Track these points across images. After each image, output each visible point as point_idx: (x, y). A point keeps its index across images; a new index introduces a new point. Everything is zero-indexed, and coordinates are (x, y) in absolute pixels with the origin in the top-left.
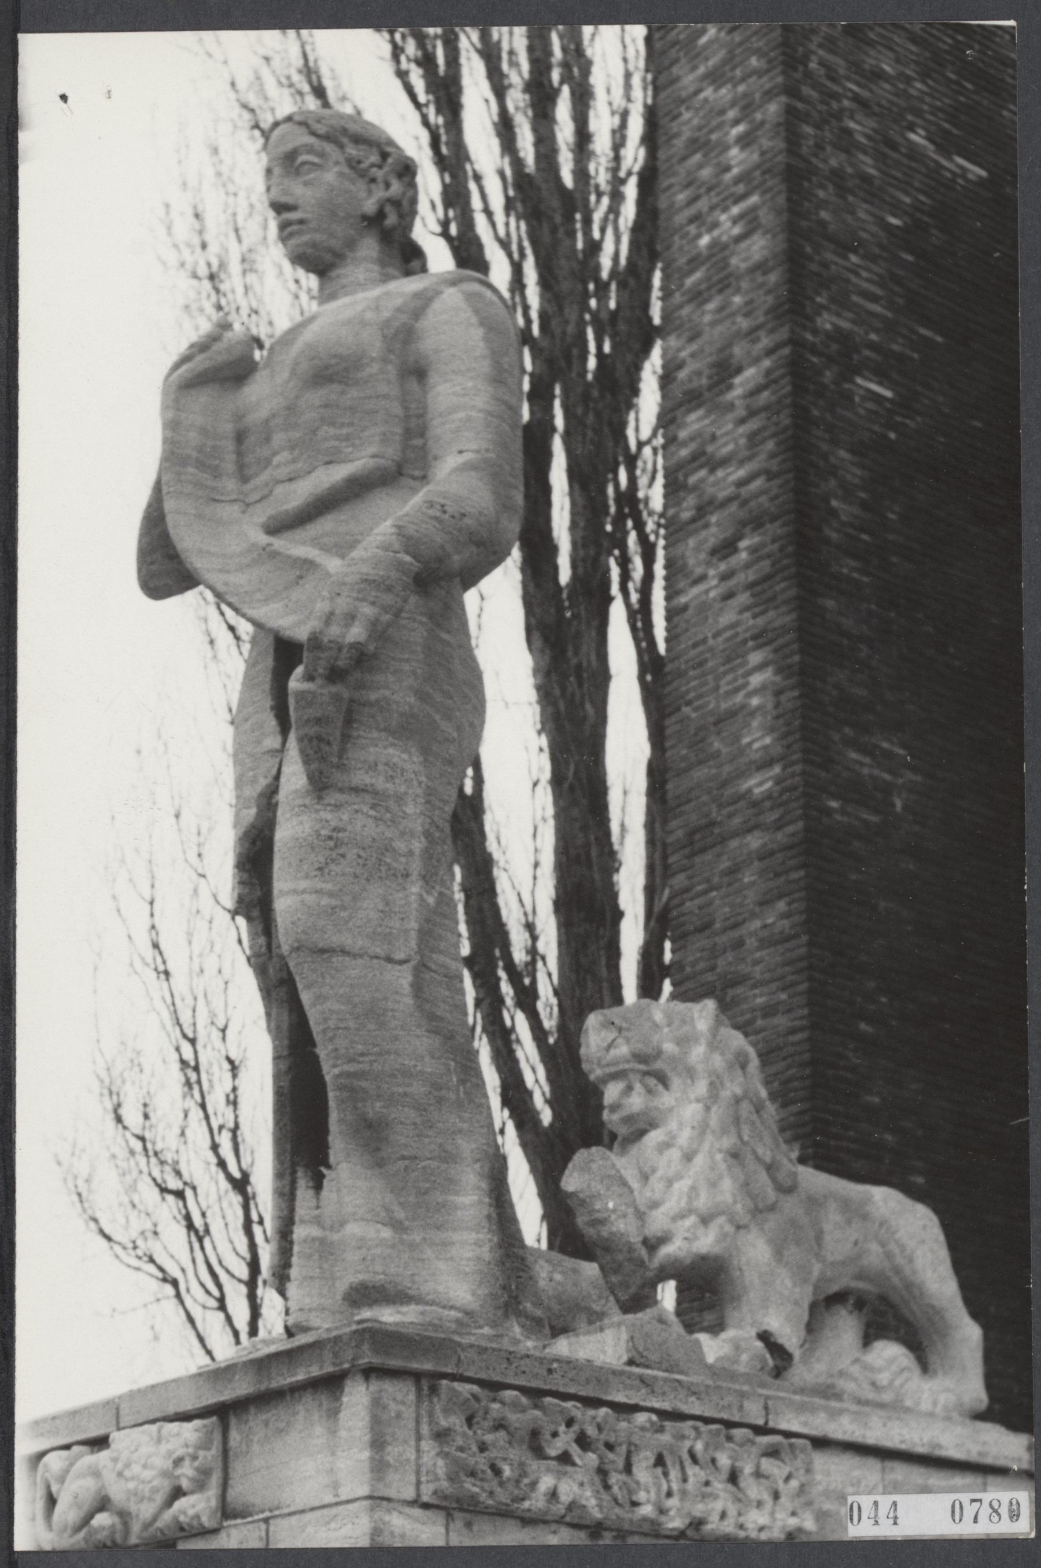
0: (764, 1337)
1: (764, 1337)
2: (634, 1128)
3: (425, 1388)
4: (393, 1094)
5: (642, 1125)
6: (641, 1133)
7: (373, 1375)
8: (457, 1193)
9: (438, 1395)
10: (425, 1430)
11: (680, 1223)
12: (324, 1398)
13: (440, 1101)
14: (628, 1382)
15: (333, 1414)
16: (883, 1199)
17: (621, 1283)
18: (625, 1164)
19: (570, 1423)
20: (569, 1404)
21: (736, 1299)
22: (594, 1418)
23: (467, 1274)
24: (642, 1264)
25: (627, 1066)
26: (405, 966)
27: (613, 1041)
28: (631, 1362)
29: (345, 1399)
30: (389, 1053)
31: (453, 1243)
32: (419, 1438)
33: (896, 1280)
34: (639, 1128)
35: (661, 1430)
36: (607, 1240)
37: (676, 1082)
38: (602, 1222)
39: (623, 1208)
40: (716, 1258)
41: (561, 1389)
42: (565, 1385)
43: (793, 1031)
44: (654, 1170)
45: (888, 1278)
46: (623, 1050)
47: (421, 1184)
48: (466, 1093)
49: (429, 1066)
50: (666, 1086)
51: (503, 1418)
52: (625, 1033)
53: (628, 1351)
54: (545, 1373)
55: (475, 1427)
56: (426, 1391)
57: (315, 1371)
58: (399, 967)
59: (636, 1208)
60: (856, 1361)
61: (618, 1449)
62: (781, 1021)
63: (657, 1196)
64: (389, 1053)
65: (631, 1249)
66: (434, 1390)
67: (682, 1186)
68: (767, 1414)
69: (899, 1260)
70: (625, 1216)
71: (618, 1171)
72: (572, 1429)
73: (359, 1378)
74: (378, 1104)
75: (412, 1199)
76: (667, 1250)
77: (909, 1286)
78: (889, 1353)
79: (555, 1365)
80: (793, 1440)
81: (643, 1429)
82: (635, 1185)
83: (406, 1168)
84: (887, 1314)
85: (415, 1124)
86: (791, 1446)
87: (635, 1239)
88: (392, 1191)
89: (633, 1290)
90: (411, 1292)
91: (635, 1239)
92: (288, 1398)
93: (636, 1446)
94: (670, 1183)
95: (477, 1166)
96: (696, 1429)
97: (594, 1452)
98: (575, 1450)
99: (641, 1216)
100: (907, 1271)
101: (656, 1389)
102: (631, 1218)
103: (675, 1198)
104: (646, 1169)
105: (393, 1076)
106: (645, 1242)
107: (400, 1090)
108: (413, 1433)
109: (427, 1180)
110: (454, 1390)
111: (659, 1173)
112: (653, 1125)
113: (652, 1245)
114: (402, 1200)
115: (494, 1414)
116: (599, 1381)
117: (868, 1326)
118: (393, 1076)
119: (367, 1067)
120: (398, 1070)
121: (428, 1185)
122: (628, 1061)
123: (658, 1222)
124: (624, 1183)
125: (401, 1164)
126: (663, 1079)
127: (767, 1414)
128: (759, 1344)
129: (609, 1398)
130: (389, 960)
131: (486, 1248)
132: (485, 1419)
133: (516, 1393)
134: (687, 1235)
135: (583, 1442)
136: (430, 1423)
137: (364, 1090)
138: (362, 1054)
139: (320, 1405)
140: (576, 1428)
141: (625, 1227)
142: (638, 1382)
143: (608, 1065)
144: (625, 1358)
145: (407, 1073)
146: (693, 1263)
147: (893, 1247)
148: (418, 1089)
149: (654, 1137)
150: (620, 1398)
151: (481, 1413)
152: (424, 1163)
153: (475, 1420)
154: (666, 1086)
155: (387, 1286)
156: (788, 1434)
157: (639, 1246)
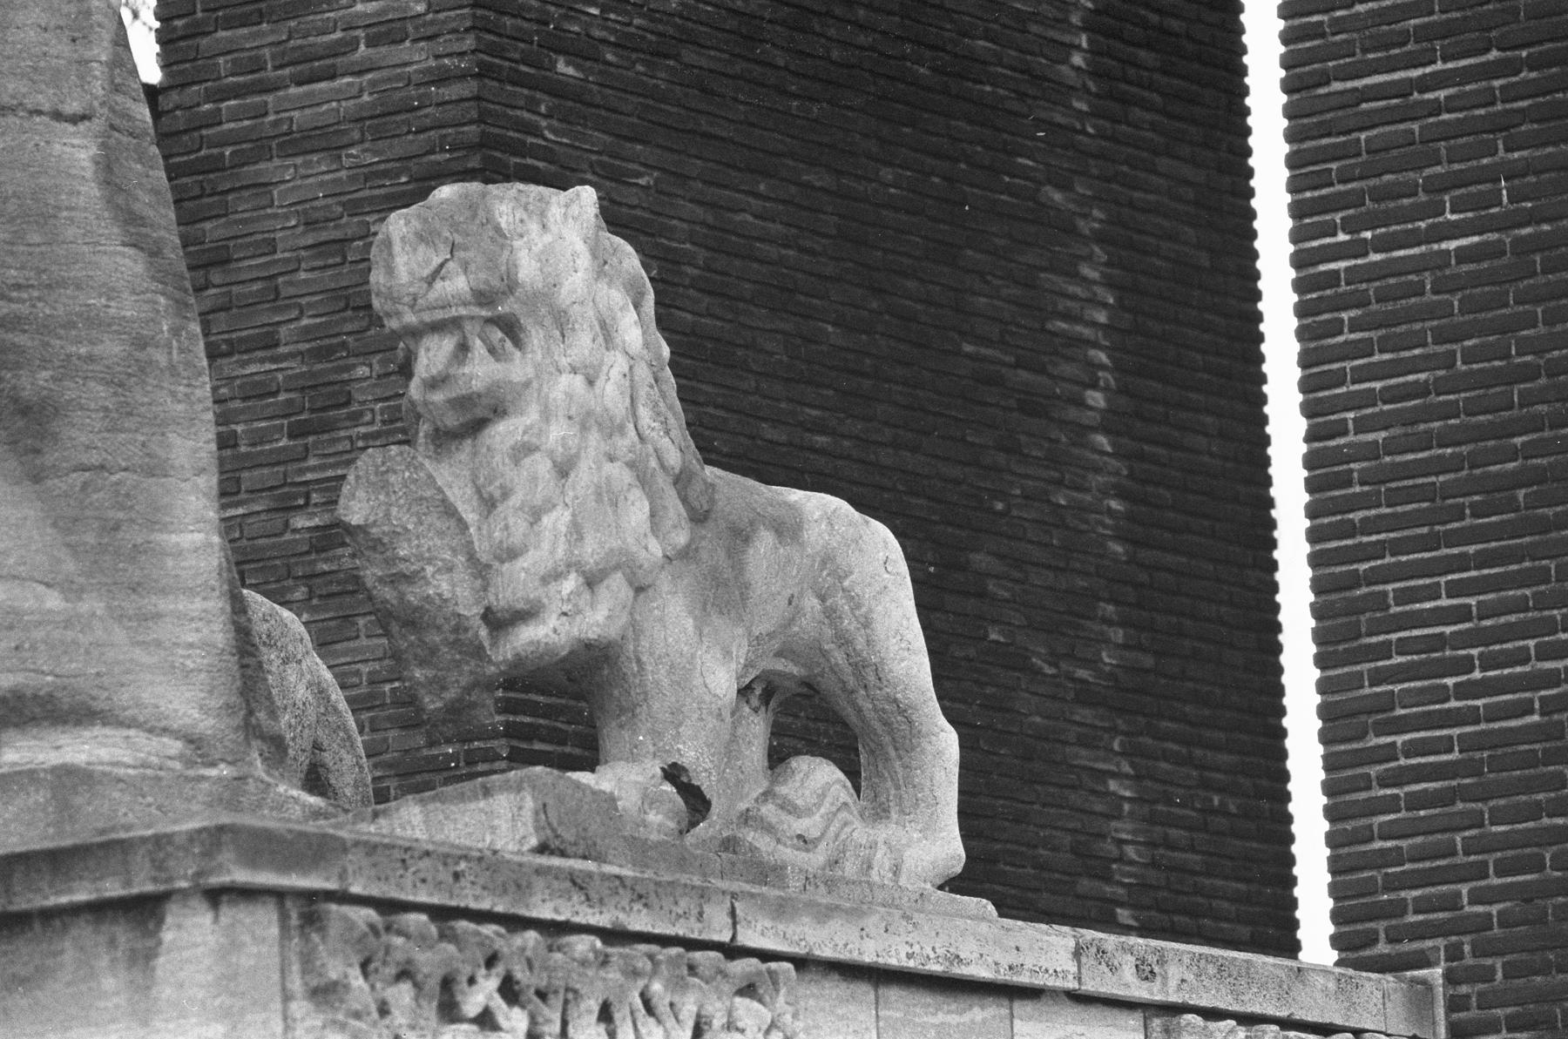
0: (673, 774)
1: (673, 774)
2: (469, 416)
3: (294, 915)
4: (69, 356)
5: (480, 413)
6: (477, 426)
7: (225, 898)
8: (165, 528)
9: (322, 929)
10: (296, 984)
11: (553, 587)
12: (123, 934)
13: (144, 368)
14: (556, 884)
15: (143, 959)
16: (822, 510)
17: (431, 682)
18: (451, 477)
19: (491, 961)
20: (489, 929)
21: (629, 712)
22: (523, 949)
23: (188, 673)
24: (478, 652)
25: (463, 311)
26: (82, 127)
27: (442, 265)
28: (542, 849)
29: (168, 936)
30: (62, 283)
31: (158, 616)
32: (287, 998)
33: (839, 657)
34: (475, 417)
35: (605, 962)
36: (417, 609)
37: (535, 337)
38: (409, 578)
39: (447, 556)
40: (610, 645)
41: (473, 905)
42: (476, 898)
43: (442, 78)
44: (506, 494)
45: (825, 654)
46: (457, 284)
47: (111, 514)
48: (181, 351)
49: (128, 308)
50: (518, 343)
51: (409, 962)
52: (460, 254)
53: (537, 829)
54: (451, 880)
55: (371, 978)
56: (295, 921)
57: (113, 889)
58: (71, 128)
59: (472, 557)
60: (767, 795)
61: (552, 999)
62: (416, 57)
63: (516, 539)
64: (62, 283)
65: (460, 626)
66: (312, 920)
67: (557, 520)
68: (734, 924)
69: (848, 623)
70: (450, 570)
71: (440, 490)
72: (494, 971)
73: (199, 904)
74: (45, 374)
75: (90, 539)
76: (529, 635)
77: (859, 667)
78: (818, 776)
79: (463, 865)
80: (773, 965)
81: (584, 963)
82: (470, 517)
83: (85, 485)
84: (812, 714)
85: (106, 409)
86: (770, 972)
87: (471, 611)
88: (54, 525)
89: (451, 694)
90: (98, 705)
91: (471, 611)
92: (37, 926)
93: (575, 992)
94: (536, 515)
95: (201, 481)
96: (651, 957)
97: (523, 1007)
98: (498, 1003)
99: (481, 571)
100: (860, 643)
101: (593, 895)
102: (462, 574)
103: (546, 546)
104: (494, 489)
105: (71, 325)
106: (488, 616)
107: (83, 351)
108: (277, 988)
109: (122, 508)
110: (345, 918)
111: (515, 500)
112: (499, 411)
113: (500, 622)
114: (73, 539)
115: (399, 956)
116: (519, 886)
117: (777, 731)
118: (71, 325)
119: (24, 309)
120: (79, 315)
121: (121, 515)
122: (465, 304)
123: (515, 583)
124: (449, 511)
125: (78, 478)
126: (511, 329)
127: (734, 924)
128: (668, 788)
129: (534, 914)
130: (58, 116)
131: (217, 627)
132: (385, 963)
133: (424, 918)
134: (565, 608)
135: (510, 991)
136: (304, 972)
137: (20, 350)
138: (18, 287)
139: (112, 943)
140: (500, 969)
141: (450, 587)
142: (568, 884)
143: (431, 308)
144: (534, 841)
145: (95, 322)
146: (571, 652)
147: (839, 600)
148: (112, 348)
149: (503, 433)
150: (545, 913)
151: (381, 954)
152: (114, 478)
153: (372, 966)
154: (518, 343)
155: (59, 695)
156: (766, 956)
157: (478, 622)
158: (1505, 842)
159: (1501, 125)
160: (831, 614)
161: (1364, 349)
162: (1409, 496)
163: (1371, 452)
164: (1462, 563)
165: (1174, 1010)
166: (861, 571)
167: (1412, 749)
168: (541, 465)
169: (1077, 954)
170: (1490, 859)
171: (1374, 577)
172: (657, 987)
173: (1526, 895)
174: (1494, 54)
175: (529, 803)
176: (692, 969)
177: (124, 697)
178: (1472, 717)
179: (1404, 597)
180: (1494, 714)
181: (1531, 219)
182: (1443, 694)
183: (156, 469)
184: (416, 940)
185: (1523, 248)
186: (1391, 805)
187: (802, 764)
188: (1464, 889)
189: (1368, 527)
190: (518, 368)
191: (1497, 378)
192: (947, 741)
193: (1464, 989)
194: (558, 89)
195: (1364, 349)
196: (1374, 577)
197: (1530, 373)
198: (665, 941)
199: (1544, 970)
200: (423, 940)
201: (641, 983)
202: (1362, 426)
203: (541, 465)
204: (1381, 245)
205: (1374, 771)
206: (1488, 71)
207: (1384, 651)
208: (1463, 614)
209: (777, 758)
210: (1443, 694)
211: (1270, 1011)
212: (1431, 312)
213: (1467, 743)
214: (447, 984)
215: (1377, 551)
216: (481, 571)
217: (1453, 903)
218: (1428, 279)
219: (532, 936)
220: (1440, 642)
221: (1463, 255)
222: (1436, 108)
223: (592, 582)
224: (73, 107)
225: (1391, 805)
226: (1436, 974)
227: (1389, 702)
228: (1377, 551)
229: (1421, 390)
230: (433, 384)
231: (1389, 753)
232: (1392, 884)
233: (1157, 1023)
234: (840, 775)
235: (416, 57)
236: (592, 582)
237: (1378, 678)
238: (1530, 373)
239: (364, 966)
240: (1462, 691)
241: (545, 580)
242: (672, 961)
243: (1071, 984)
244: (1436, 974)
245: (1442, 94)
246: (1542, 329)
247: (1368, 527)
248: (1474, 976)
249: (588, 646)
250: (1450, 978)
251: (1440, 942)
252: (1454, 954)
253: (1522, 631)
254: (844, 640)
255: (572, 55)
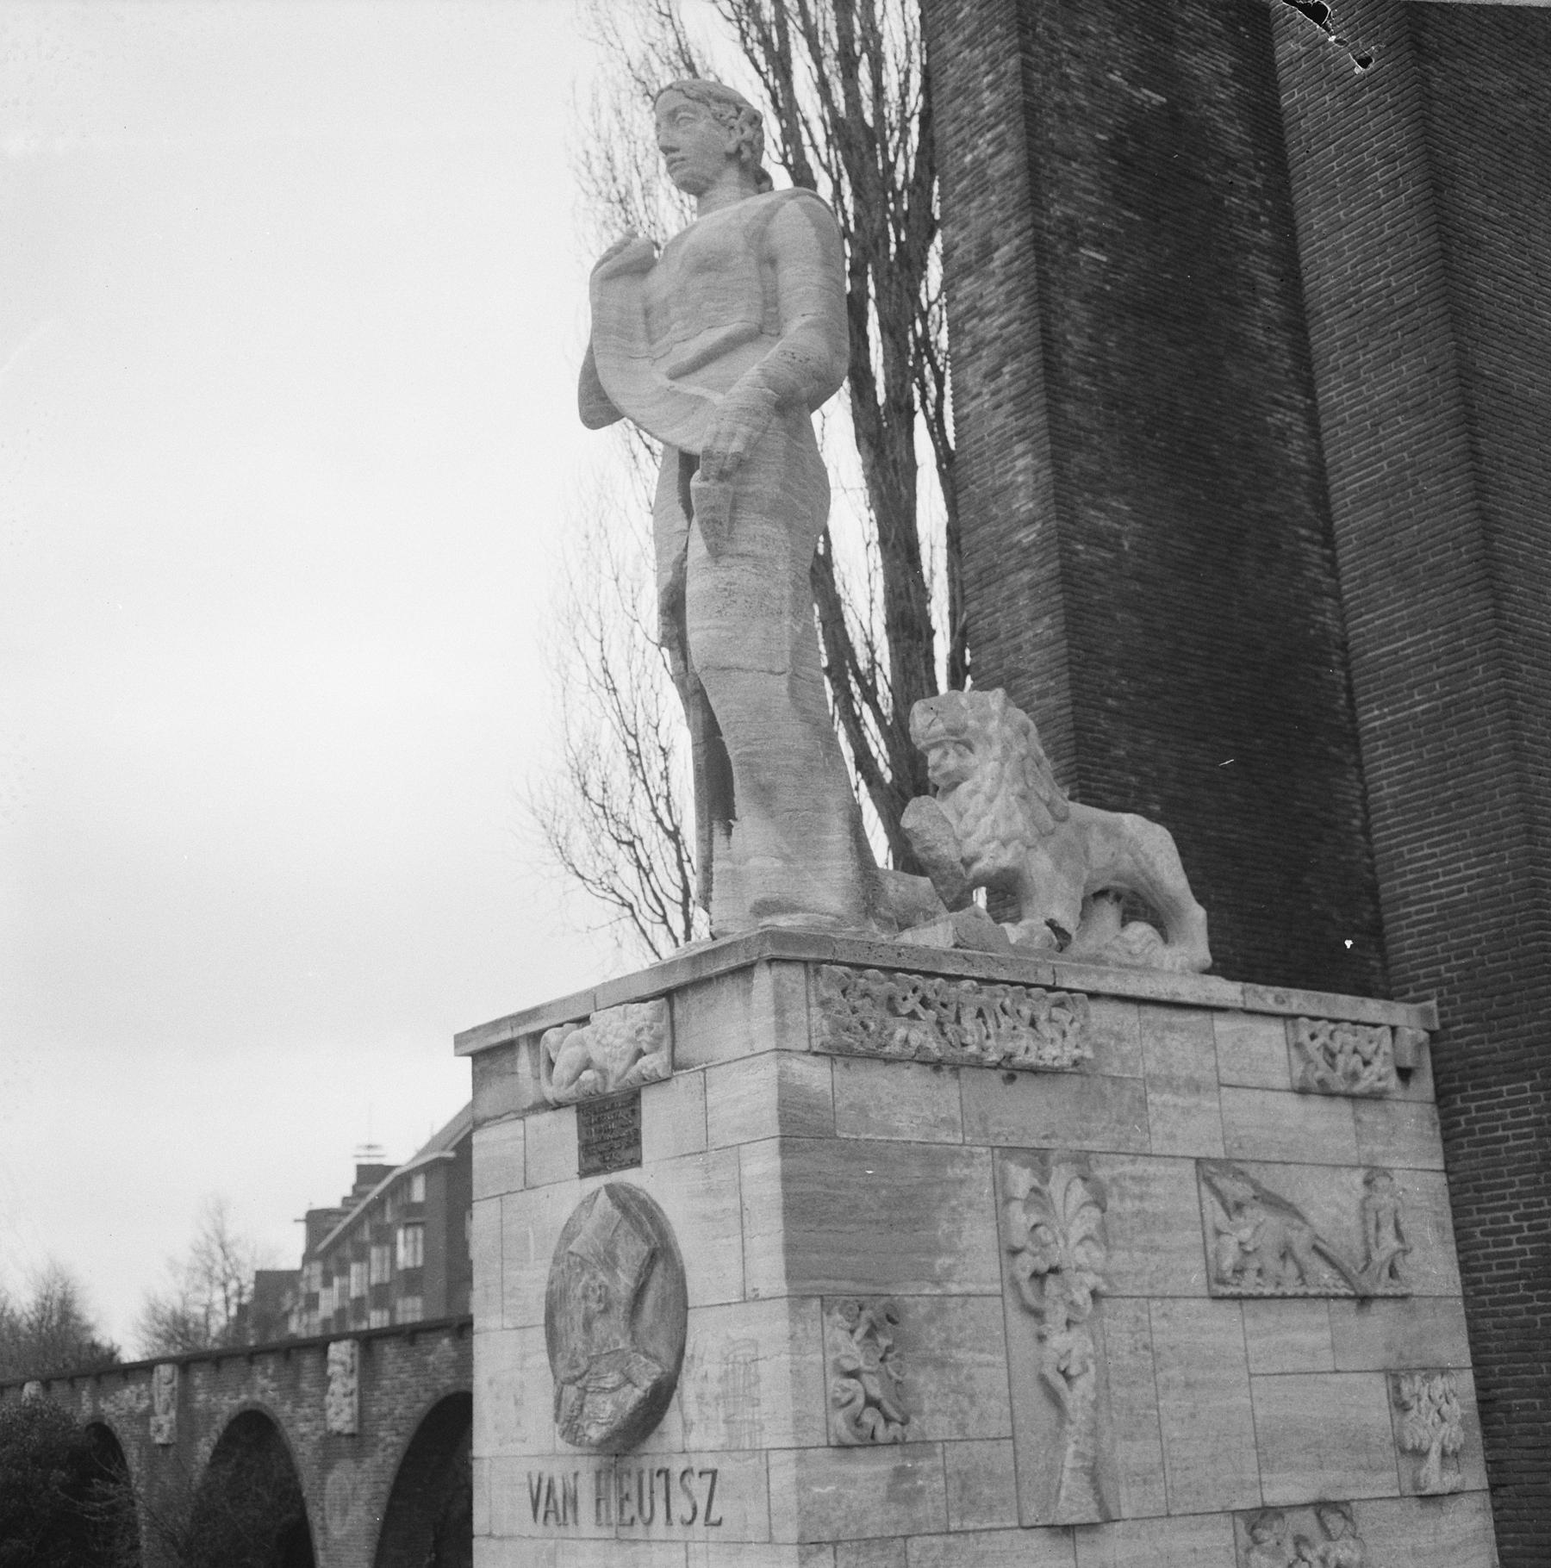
0: (1051, 923)
1: (1051, 923)
8: (827, 833)
10: (813, 1000)
12: (740, 981)
16: (1131, 822)
18: (945, 806)
20: (914, 977)
21: (1029, 898)
28: (956, 946)
32: (809, 1006)
33: (1143, 879)
37: (979, 747)
43: (1060, 708)
50: (972, 751)
57: (733, 963)
62: (1051, 701)
63: (969, 828)
67: (987, 820)
77: (1152, 883)
81: (967, 992)
82: (954, 822)
94: (978, 818)
98: (919, 1009)
99: (959, 843)
102: (952, 844)
106: (962, 861)
112: (964, 779)
113: (967, 863)
124: (945, 820)
128: (1047, 929)
130: (771, 672)
135: (924, 1002)
140: (919, 993)
141: (947, 851)
147: (1140, 856)
149: (965, 787)
150: (950, 971)
154: (972, 751)
156: (1070, 991)
158: (1458, 947)
159: (1435, 659)
160: (1137, 862)
161: (1388, 755)
162: (1410, 810)
163: (1393, 796)
164: (1431, 835)
165: (1296, 1017)
166: (1150, 847)
167: (1417, 913)
168: (980, 798)
169: (1243, 992)
170: (1452, 954)
171: (1398, 845)
172: (1008, 1002)
173: (1467, 967)
174: (1429, 632)
175: (951, 928)
176: (1029, 995)
177: (808, 901)
178: (1441, 897)
179: (1410, 851)
180: (1449, 895)
181: (1449, 693)
182: (1428, 889)
183: (820, 808)
184: (882, 987)
185: (1447, 706)
186: (1410, 936)
187: (1132, 925)
188: (1442, 967)
189: (1394, 825)
190: (972, 760)
191: (1444, 759)
192: (1198, 913)
193: (1445, 1008)
194: (1108, 710)
195: (1388, 755)
196: (1398, 845)
197: (1453, 755)
198: (1013, 984)
199: (1476, 998)
200: (876, 980)
201: (999, 1000)
202: (1390, 785)
203: (980, 798)
204: (1392, 713)
205: (1403, 923)
206: (1427, 639)
207: (1404, 874)
208: (1433, 855)
209: (1124, 923)
210: (1428, 889)
211: (1347, 1017)
212: (1412, 737)
213: (1440, 908)
214: (891, 999)
215: (1395, 836)
216: (959, 843)
217: (1438, 974)
218: (1410, 724)
219: (939, 980)
220: (1425, 868)
221: (1423, 712)
222: (1408, 657)
223: (1004, 844)
224: (777, 670)
225: (1410, 936)
226: (1433, 1004)
227: (1406, 895)
228: (1395, 836)
229: (1412, 768)
230: (935, 768)
231: (1408, 915)
232: (1414, 968)
233: (1289, 1023)
234: (1150, 928)
235: (1051, 701)
236: (1004, 844)
237: (1403, 885)
238: (1453, 755)
239: (844, 992)
240: (1436, 887)
241: (982, 844)
242: (1020, 992)
243: (1241, 1005)
244: (1433, 1004)
245: (1409, 651)
246: (1456, 737)
247: (1394, 825)
248: (1449, 1003)
249: (1005, 870)
250: (1439, 1004)
251: (1435, 990)
252: (1440, 994)
253: (1458, 859)
254: (1144, 872)
255: (1117, 697)
